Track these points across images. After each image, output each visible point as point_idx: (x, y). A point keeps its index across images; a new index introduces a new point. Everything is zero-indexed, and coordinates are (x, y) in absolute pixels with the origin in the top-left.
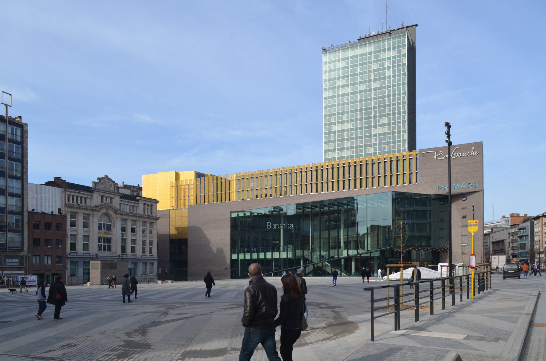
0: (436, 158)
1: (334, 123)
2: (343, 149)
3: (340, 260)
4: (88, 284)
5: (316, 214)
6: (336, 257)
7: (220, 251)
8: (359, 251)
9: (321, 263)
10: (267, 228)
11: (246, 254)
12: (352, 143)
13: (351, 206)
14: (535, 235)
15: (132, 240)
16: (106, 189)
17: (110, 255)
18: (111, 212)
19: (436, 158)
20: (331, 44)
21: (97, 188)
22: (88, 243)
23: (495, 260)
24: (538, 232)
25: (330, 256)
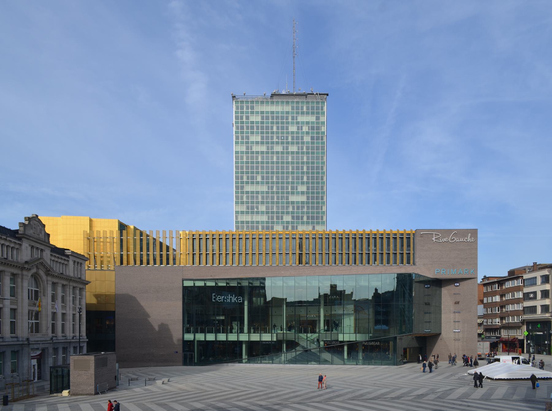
0: (434, 240)
1: (247, 183)
2: (257, 213)
4: (65, 393)
7: (164, 328)
10: (213, 301)
11: (207, 334)
12: (267, 208)
15: (11, 309)
16: (36, 236)
17: (42, 339)
18: (42, 273)
20: (244, 93)
21: (26, 233)
22: (64, 322)
23: (480, 346)
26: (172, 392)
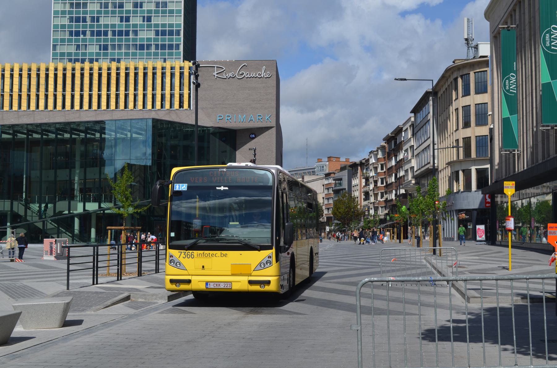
0: (216, 75)
3: (71, 218)
5: (36, 143)
6: (67, 212)
8: (103, 205)
9: (42, 222)
13: (121, 134)
14: (353, 189)
19: (216, 75)
24: (355, 186)
25: (57, 211)
26: (18, 270)
